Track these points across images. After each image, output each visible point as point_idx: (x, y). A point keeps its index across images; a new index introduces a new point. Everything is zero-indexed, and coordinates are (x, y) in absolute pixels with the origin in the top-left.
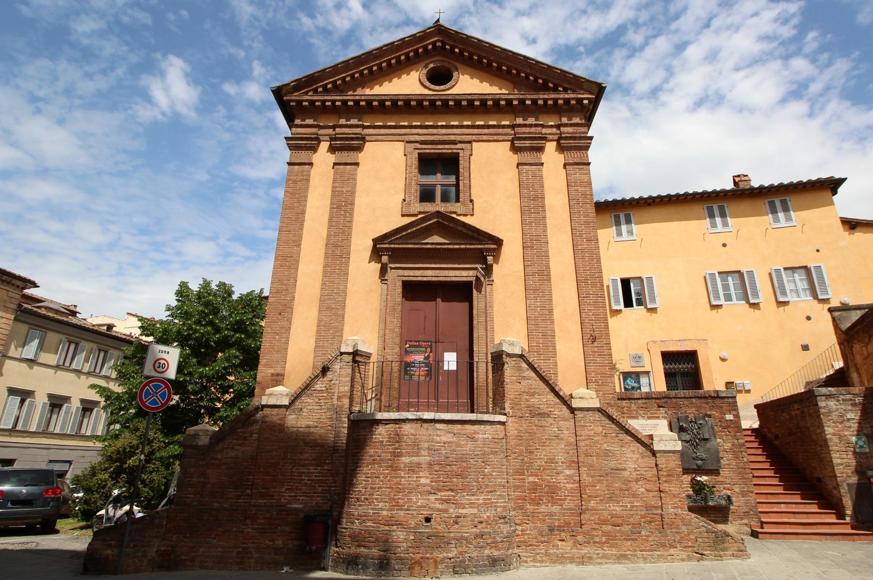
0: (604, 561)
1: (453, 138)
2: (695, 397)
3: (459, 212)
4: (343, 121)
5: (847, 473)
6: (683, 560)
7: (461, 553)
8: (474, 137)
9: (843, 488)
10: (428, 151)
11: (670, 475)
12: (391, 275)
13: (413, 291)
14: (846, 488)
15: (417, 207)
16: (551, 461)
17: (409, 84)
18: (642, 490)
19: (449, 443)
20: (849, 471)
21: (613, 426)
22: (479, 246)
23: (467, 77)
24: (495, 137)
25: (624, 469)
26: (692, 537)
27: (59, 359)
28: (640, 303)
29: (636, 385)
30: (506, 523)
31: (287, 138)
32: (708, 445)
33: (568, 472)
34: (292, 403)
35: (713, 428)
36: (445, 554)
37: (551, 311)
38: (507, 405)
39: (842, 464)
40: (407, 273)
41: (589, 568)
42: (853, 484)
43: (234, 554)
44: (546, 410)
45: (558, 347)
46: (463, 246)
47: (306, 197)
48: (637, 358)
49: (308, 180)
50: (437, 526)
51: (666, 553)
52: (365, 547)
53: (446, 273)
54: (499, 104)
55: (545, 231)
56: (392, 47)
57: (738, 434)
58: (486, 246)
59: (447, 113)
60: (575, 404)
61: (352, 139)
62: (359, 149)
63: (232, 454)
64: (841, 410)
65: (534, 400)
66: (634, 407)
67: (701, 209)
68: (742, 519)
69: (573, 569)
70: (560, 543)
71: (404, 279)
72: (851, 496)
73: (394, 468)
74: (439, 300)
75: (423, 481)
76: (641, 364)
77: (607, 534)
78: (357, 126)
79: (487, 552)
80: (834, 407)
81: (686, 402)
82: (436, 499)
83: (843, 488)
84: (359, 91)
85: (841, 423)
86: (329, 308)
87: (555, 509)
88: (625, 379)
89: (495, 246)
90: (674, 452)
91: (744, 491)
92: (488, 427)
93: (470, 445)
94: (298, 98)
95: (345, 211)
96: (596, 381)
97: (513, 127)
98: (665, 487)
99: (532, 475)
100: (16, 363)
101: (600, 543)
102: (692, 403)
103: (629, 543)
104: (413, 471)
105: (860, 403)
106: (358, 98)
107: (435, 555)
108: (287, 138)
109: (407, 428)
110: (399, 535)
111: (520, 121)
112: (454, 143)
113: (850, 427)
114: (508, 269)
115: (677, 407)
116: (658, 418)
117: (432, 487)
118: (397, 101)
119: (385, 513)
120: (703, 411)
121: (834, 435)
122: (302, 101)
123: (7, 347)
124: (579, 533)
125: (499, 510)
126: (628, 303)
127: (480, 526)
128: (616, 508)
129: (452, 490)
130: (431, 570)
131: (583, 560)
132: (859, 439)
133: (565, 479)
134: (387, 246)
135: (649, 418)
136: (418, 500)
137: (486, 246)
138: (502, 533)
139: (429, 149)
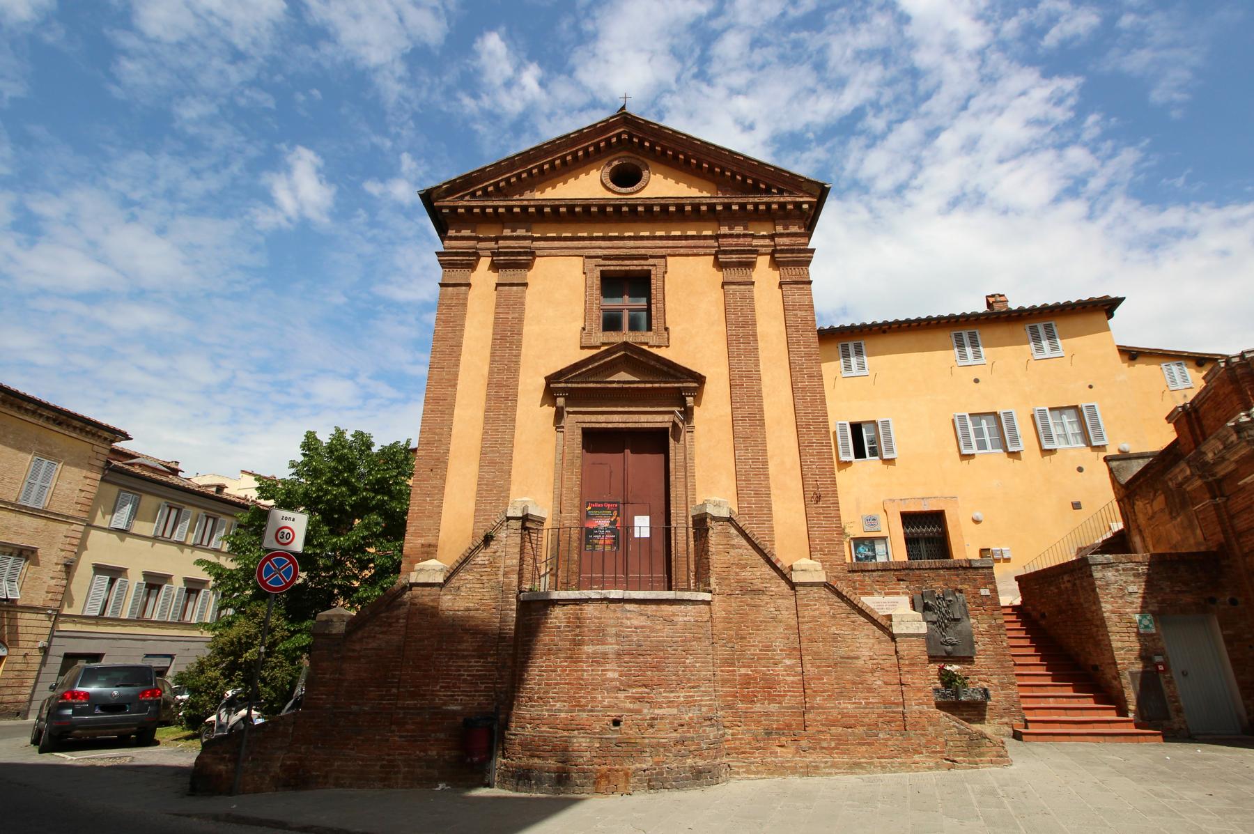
0: (833, 771)
1: (643, 251)
3: (651, 343)
4: (507, 232)
6: (930, 768)
7: (657, 763)
8: (669, 251)
12: (568, 420)
15: (600, 337)
16: (767, 648)
17: (589, 186)
18: (879, 683)
20: (1132, 657)
21: (843, 605)
23: (659, 177)
24: (695, 251)
25: (857, 658)
26: (941, 740)
27: (157, 529)
28: (874, 452)
29: (870, 553)
30: (713, 725)
32: (959, 627)
33: (788, 662)
35: (965, 606)
36: (638, 765)
37: (765, 463)
38: (712, 580)
40: (587, 418)
41: (814, 781)
43: (378, 768)
44: (760, 586)
47: (463, 325)
48: (872, 521)
49: (465, 305)
52: (539, 757)
54: (699, 210)
55: (757, 365)
59: (635, 221)
60: (796, 578)
61: (519, 254)
62: (528, 266)
63: (374, 645)
65: (746, 574)
66: (868, 581)
67: (947, 336)
68: (1002, 717)
69: (795, 781)
70: (779, 749)
73: (573, 659)
74: (627, 451)
75: (610, 675)
77: (838, 739)
79: (689, 761)
82: (627, 697)
85: (1121, 597)
86: (492, 463)
87: (773, 707)
88: (856, 547)
92: (690, 608)
93: (668, 630)
95: (511, 343)
96: (821, 550)
98: (907, 678)
99: (744, 667)
102: (939, 575)
103: (864, 748)
104: (597, 662)
106: (525, 203)
107: (626, 766)
109: (589, 609)
112: (644, 257)
114: (713, 413)
115: (922, 580)
116: (898, 594)
117: (621, 682)
119: (563, 715)
120: (952, 585)
121: (1113, 612)
124: (803, 737)
125: (704, 709)
126: (859, 453)
127: (680, 730)
128: (848, 706)
130: (621, 785)
131: (808, 771)
133: (784, 669)
135: (887, 594)
138: (708, 738)
139: (614, 266)
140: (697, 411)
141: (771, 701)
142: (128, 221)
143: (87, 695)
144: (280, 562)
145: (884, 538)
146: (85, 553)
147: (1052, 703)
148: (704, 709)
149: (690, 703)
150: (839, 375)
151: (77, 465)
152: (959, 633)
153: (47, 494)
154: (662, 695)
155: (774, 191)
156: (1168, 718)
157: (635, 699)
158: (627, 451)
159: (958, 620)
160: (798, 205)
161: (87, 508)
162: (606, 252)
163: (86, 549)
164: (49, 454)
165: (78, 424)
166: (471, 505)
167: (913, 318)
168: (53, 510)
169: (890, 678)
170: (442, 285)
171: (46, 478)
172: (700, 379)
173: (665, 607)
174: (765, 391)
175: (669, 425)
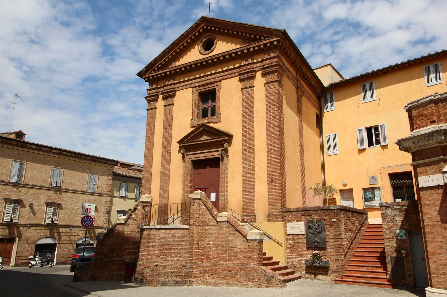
0: (222, 285)
1: (212, 80)
2: (319, 210)
4: (167, 83)
5: (391, 251)
6: (252, 287)
7: (165, 278)
8: (222, 78)
9: (388, 259)
10: (202, 90)
11: (253, 250)
12: (187, 158)
13: (198, 164)
14: (390, 259)
15: (198, 122)
16: (208, 244)
17: (195, 55)
18: (242, 257)
19: (165, 237)
20: (393, 250)
21: (233, 229)
22: (221, 139)
23: (220, 42)
24: (232, 76)
25: (236, 248)
26: (258, 277)
27: (136, 195)
28: (378, 142)
29: (372, 196)
30: (186, 268)
31: (146, 97)
32: (321, 236)
33: (214, 249)
34: (126, 222)
35: (324, 226)
37: (253, 168)
39: (389, 246)
40: (193, 156)
41: (216, 288)
42: (393, 257)
45: (256, 187)
46: (214, 140)
48: (373, 179)
49: (155, 117)
50: (159, 268)
51: (246, 284)
53: (208, 154)
56: (183, 37)
57: (337, 229)
58: (224, 139)
61: (170, 92)
62: (173, 96)
63: (109, 242)
64: (392, 215)
65: (204, 218)
66: (291, 216)
67: (422, 69)
68: (334, 273)
70: (208, 277)
71: (192, 159)
72: (391, 264)
73: (148, 247)
74: (208, 168)
75: (156, 252)
76: (375, 183)
77: (225, 275)
78: (172, 84)
79: (175, 279)
80: (389, 213)
81: (314, 212)
83: (388, 259)
84: (174, 65)
85: (392, 222)
86: (164, 177)
87: (208, 264)
88: (365, 193)
89: (227, 138)
90: (256, 240)
91: (336, 259)
92: (180, 231)
93: (173, 238)
94: (147, 76)
96: (272, 204)
97: (239, 67)
100: (118, 199)
101: (222, 278)
102: (317, 213)
103: (233, 278)
105: (404, 211)
106: (170, 69)
108: (146, 97)
109: (152, 231)
110: (147, 271)
111: (244, 63)
112: (213, 83)
113: (397, 225)
114: (235, 149)
115: (310, 215)
116: (301, 221)
118: (186, 66)
120: (322, 217)
121: (387, 229)
122: (149, 77)
123: (112, 192)
124: (215, 274)
126: (370, 144)
127: (174, 269)
128: (230, 264)
129: (165, 255)
131: (214, 284)
132: (400, 232)
133: (213, 251)
134: (183, 145)
135: (297, 221)
136: (154, 259)
137: (224, 139)
138: (182, 272)
139: (203, 89)
140: (230, 149)
141: (208, 262)
142: (146, 38)
143: (78, 255)
144: (88, 218)
145: (379, 188)
146: (113, 206)
147: (365, 269)
148: (183, 263)
149: (178, 261)
150: (361, 103)
151: (103, 175)
152: (320, 238)
153: (96, 187)
154: (169, 258)
155: (262, 38)
156: (404, 278)
157: (162, 259)
158: (208, 168)
159: (320, 232)
160: (272, 43)
161: (110, 190)
162: (199, 84)
163: (400, 149)
164: (93, 173)
165: (100, 160)
166: (158, 193)
167: (399, 63)
168: (99, 192)
169: (245, 255)
170: (148, 110)
171: (94, 182)
172: (230, 137)
173: (172, 231)
174: (256, 136)
175: (220, 156)
